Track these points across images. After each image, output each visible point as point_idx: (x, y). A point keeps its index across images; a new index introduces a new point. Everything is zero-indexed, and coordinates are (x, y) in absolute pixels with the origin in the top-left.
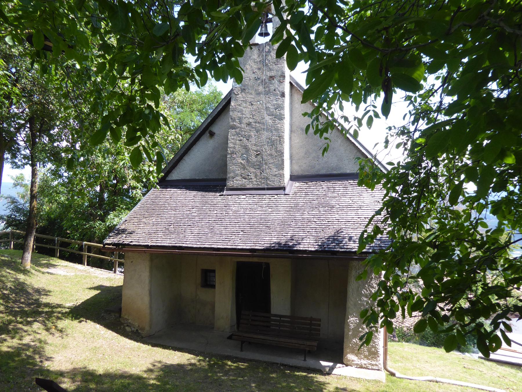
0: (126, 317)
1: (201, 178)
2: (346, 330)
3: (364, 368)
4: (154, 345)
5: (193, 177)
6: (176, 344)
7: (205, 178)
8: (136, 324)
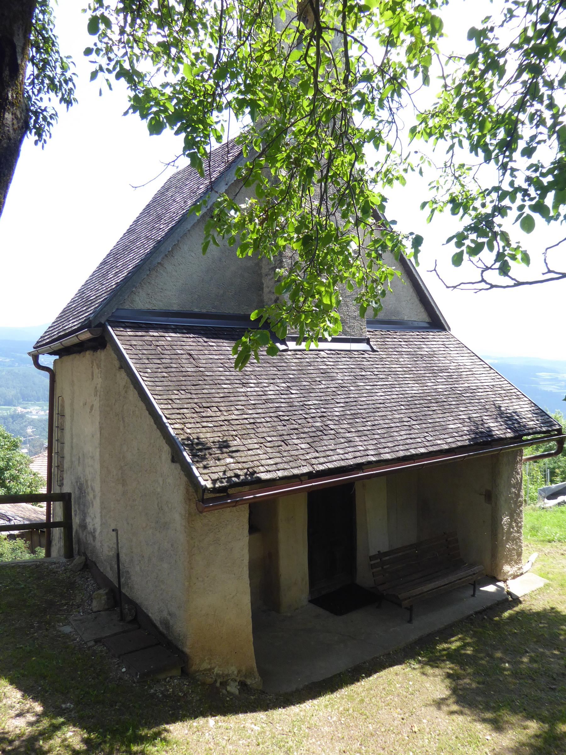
0: (205, 666)
1: (204, 311)
2: (500, 536)
3: (518, 576)
4: (331, 685)
5: (187, 308)
6: (342, 664)
7: (214, 310)
8: (233, 670)
